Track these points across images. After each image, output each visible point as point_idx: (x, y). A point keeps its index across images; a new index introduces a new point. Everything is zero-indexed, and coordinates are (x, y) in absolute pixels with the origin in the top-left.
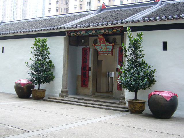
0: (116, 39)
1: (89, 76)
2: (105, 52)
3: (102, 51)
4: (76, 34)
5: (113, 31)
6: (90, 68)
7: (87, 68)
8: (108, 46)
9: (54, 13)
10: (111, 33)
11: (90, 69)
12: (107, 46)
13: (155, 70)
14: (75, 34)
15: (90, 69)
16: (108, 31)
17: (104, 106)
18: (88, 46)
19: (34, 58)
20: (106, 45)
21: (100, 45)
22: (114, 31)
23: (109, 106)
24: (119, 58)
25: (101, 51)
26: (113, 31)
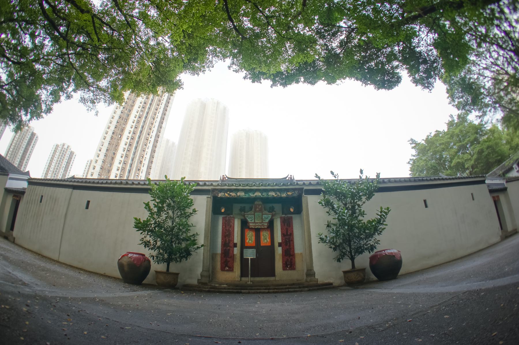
0: (274, 208)
1: (234, 255)
2: (257, 223)
3: (254, 222)
4: (229, 194)
5: (287, 194)
6: (236, 244)
7: (231, 245)
8: (265, 216)
9: (96, 176)
10: (285, 196)
11: (235, 245)
12: (263, 216)
13: (136, 219)
14: (226, 195)
15: (235, 245)
16: (280, 193)
17: (282, 289)
18: (232, 214)
19: (229, 61)
20: (262, 215)
21: (254, 214)
22: (289, 193)
23: (32, 192)
24: (223, 226)
25: (252, 223)
26: (287, 194)
